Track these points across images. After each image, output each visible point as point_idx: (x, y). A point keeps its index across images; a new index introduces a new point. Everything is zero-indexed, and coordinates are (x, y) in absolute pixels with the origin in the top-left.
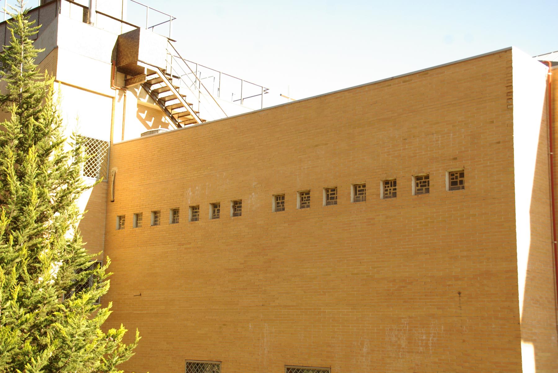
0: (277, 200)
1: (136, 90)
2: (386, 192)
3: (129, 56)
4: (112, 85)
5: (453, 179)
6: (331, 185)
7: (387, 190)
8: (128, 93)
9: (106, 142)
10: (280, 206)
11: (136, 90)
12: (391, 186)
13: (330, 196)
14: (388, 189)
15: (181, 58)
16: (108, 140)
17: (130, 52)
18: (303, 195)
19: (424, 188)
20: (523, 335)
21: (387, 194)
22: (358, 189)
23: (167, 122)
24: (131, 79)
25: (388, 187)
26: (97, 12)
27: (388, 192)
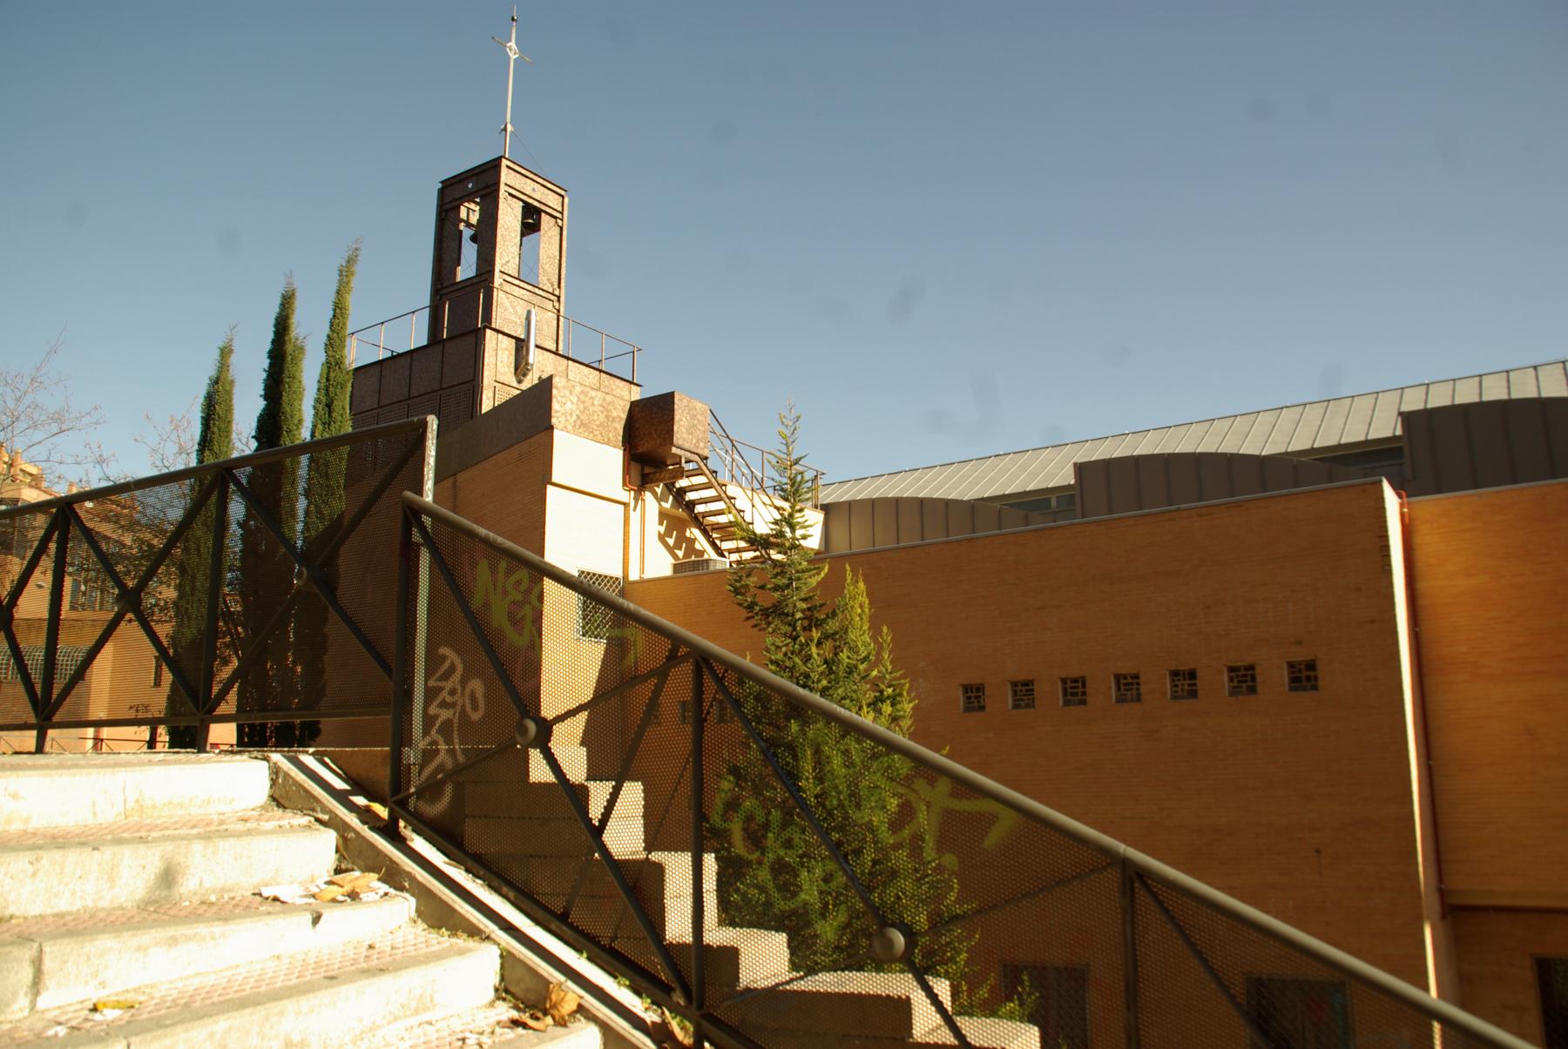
0: (967, 693)
1: (656, 489)
2: (1175, 689)
3: (655, 436)
4: (624, 484)
5: (1293, 673)
6: (1075, 673)
7: (1176, 686)
8: (648, 496)
9: (617, 579)
10: (973, 702)
11: (656, 489)
12: (1184, 679)
13: (1069, 691)
14: (1180, 683)
15: (728, 437)
16: (619, 574)
17: (656, 430)
18: (1016, 686)
19: (1244, 685)
20: (560, 787)
21: (1177, 692)
22: (1122, 681)
23: (693, 537)
24: (654, 473)
25: (1179, 680)
26: (537, 346)
27: (1179, 689)
